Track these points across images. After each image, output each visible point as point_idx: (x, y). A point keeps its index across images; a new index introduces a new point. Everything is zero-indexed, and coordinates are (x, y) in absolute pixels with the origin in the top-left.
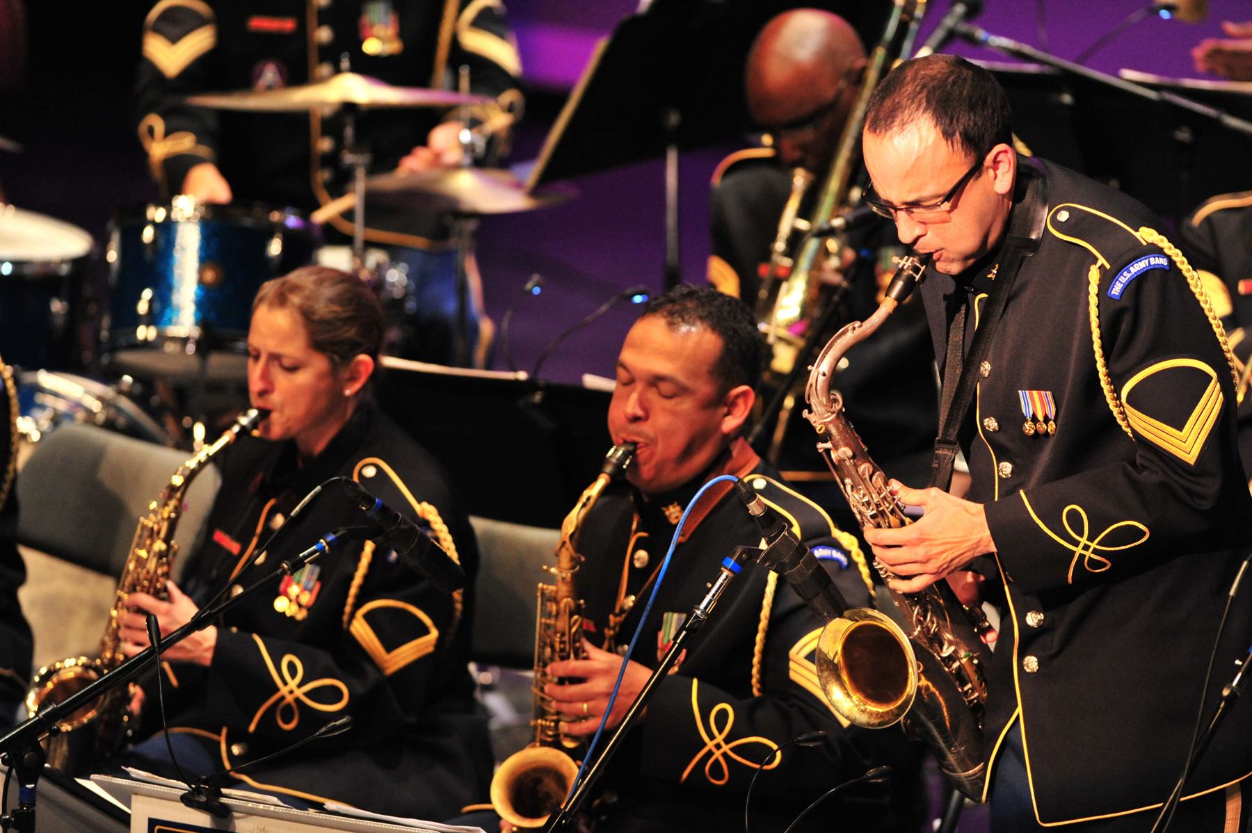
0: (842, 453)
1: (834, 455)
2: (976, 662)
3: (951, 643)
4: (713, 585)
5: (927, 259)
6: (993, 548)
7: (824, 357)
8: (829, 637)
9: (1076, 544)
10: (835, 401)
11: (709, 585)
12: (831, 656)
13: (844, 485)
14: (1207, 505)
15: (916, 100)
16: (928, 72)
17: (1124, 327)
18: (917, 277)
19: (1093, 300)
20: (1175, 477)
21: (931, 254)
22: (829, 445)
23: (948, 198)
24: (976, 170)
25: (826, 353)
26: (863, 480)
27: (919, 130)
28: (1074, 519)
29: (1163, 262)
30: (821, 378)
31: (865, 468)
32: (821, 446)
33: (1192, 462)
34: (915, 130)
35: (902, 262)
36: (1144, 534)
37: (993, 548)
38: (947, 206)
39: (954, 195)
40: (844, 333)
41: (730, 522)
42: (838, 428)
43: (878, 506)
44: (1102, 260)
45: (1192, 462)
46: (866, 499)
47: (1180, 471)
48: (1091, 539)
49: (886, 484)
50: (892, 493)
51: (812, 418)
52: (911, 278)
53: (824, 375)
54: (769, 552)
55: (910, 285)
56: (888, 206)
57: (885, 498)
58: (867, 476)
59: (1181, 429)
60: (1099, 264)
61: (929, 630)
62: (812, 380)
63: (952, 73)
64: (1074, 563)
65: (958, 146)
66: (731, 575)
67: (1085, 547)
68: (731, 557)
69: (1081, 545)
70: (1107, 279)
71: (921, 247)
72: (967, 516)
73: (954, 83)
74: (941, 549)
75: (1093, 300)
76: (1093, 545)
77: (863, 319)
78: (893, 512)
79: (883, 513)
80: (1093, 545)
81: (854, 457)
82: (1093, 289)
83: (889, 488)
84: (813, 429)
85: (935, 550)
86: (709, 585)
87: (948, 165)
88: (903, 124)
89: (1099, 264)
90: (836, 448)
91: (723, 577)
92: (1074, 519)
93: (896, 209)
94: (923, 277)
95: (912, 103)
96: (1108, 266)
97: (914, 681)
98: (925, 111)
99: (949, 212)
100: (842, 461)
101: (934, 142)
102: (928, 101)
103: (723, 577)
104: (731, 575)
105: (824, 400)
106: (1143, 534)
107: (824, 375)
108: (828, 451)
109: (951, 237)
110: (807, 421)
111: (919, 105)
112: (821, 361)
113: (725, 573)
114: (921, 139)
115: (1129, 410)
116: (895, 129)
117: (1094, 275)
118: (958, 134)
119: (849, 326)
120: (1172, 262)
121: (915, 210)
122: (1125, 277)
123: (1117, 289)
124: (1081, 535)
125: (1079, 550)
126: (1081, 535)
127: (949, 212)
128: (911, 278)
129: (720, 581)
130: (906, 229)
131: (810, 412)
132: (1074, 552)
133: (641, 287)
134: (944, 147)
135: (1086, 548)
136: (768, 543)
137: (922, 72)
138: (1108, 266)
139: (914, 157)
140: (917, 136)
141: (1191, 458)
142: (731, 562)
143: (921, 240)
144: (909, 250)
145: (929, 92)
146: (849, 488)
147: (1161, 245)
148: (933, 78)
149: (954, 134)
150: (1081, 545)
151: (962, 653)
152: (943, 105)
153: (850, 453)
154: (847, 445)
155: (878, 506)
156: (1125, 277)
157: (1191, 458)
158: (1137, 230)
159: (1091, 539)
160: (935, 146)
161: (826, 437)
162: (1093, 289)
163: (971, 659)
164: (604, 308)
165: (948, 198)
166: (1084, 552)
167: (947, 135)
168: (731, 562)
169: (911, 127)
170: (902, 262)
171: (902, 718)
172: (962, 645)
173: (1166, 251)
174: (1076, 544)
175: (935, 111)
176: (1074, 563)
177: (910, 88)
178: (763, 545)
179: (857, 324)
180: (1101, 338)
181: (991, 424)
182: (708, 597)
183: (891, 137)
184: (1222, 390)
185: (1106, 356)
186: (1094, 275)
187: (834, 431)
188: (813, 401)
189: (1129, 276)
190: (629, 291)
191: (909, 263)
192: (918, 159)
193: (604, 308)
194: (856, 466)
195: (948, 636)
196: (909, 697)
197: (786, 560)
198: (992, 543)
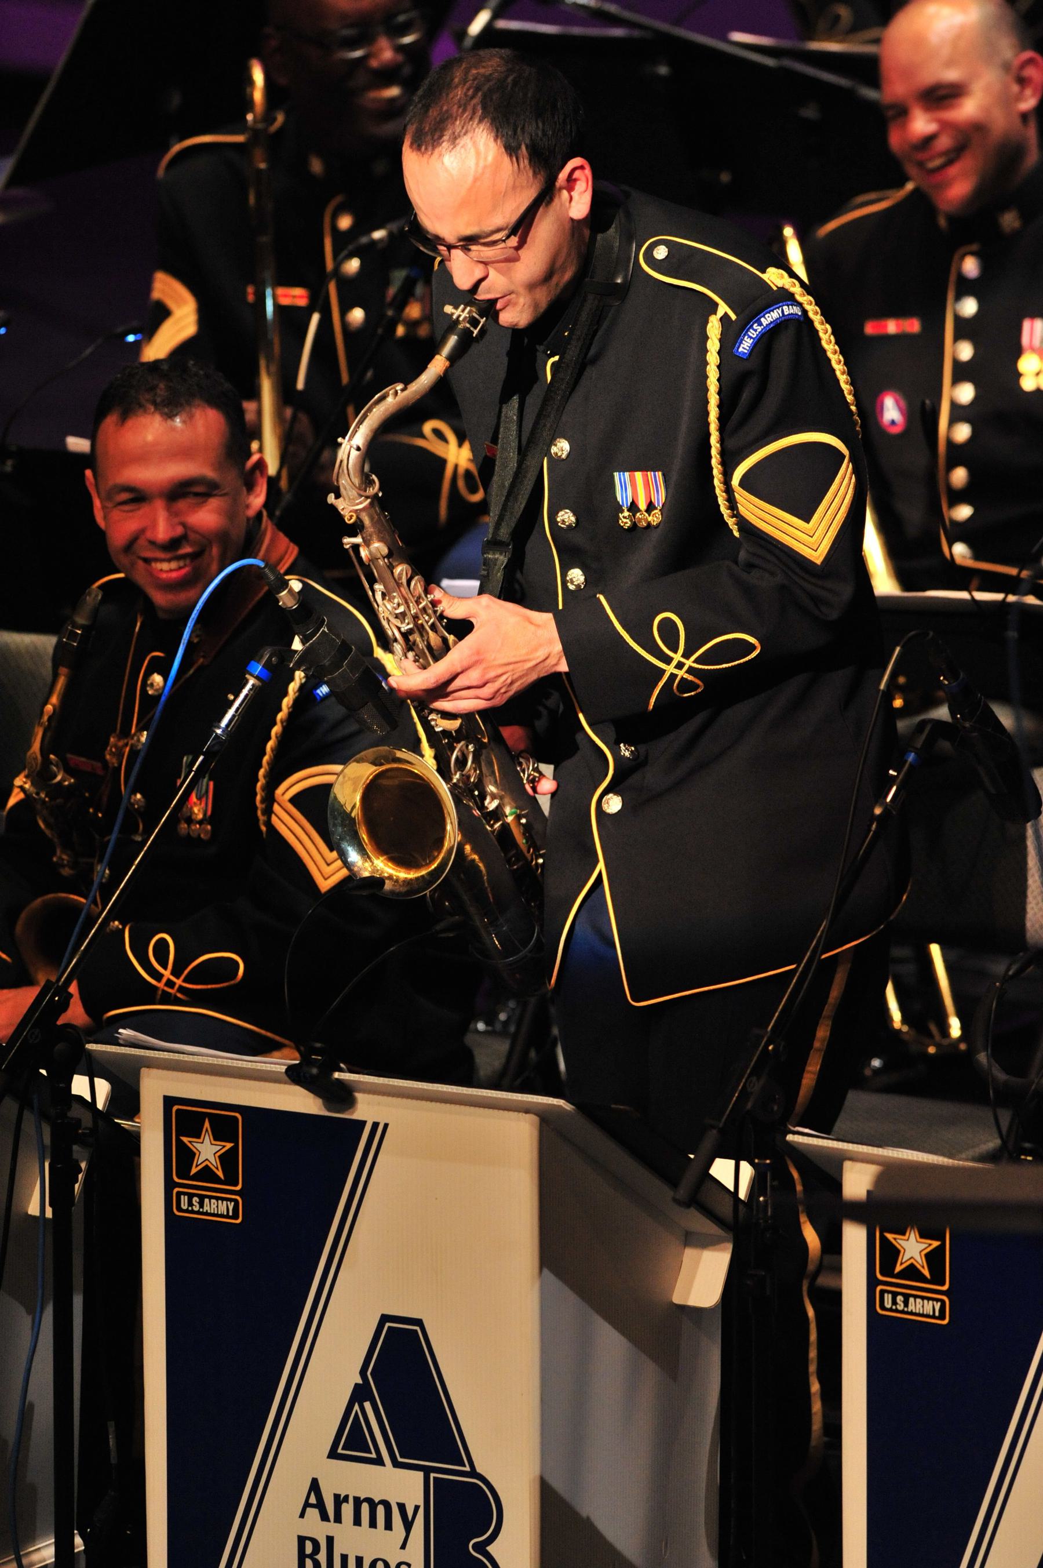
0: (373, 549)
1: (364, 553)
2: (524, 821)
3: (494, 797)
4: (236, 696)
5: (490, 309)
6: (563, 667)
7: (358, 426)
8: (349, 782)
9: (668, 660)
10: (372, 482)
11: (231, 697)
12: (348, 809)
13: (373, 591)
14: (834, 615)
15: (470, 108)
16: (482, 71)
17: (746, 396)
18: (476, 332)
19: (713, 358)
20: (797, 579)
21: (494, 301)
22: (358, 540)
23: (513, 232)
24: (546, 196)
25: (361, 422)
26: (399, 585)
27: (475, 144)
28: (668, 631)
29: (796, 310)
30: (354, 454)
31: (401, 569)
32: (348, 541)
33: (819, 562)
34: (470, 144)
35: (457, 313)
36: (754, 648)
37: (563, 667)
38: (514, 241)
39: (522, 227)
40: (383, 398)
41: (245, 620)
42: (372, 518)
43: (415, 618)
44: (723, 308)
45: (819, 562)
46: (401, 609)
47: (798, 570)
48: (686, 655)
49: (427, 592)
50: (434, 603)
51: (341, 505)
52: (467, 333)
53: (358, 449)
54: (306, 653)
55: (466, 341)
56: (434, 241)
57: (424, 610)
58: (404, 580)
59: (808, 522)
60: (720, 313)
61: (469, 777)
62: (342, 454)
63: (510, 71)
64: (661, 684)
65: (525, 162)
66: (258, 683)
67: (678, 665)
68: (258, 662)
69: (674, 663)
70: (731, 333)
71: (482, 295)
72: (532, 628)
73: (515, 83)
74: (500, 671)
75: (713, 358)
76: (689, 663)
77: (407, 382)
78: (433, 627)
79: (421, 629)
80: (689, 663)
81: (390, 555)
82: (713, 345)
83: (430, 597)
84: (341, 517)
85: (492, 674)
86: (231, 697)
87: (514, 187)
88: (454, 139)
89: (720, 313)
90: (367, 543)
91: (249, 686)
92: (668, 628)
93: (450, 247)
94: (483, 332)
95: (464, 111)
96: (733, 317)
97: (452, 834)
98: (480, 121)
99: (518, 248)
100: (373, 559)
101: (495, 158)
102: (484, 108)
103: (249, 686)
104: (258, 683)
105: (357, 481)
106: (753, 648)
107: (358, 449)
108: (356, 547)
109: (511, 284)
110: (333, 508)
111: (474, 113)
112: (355, 432)
113: (252, 681)
114: (478, 153)
115: (743, 497)
116: (445, 144)
117: (714, 328)
118: (523, 147)
119: (390, 390)
120: (805, 312)
121: (473, 248)
122: (756, 331)
123: (745, 346)
124: (675, 650)
125: (670, 669)
126: (675, 650)
127: (518, 248)
128: (467, 333)
129: (245, 691)
130: (462, 270)
131: (338, 496)
132: (664, 671)
133: (135, 324)
134: (507, 165)
135: (680, 665)
136: (303, 642)
137: (474, 72)
138: (733, 317)
139: (470, 179)
140: (473, 151)
141: (818, 556)
142: (257, 668)
143: (483, 284)
144: (469, 296)
145: (484, 97)
146: (379, 596)
147: (792, 290)
148: (488, 78)
149: (519, 147)
150: (674, 663)
151: (508, 810)
152: (504, 115)
153: (385, 551)
154: (381, 540)
155: (415, 618)
156: (756, 331)
157: (818, 556)
158: (764, 272)
159: (686, 655)
160: (496, 167)
161: (355, 529)
162: (713, 345)
163: (518, 817)
164: (89, 351)
165: (513, 232)
166: (676, 671)
167: (511, 150)
168: (257, 668)
169: (465, 141)
170: (457, 313)
171: (427, 892)
172: (507, 800)
173: (798, 298)
174: (668, 660)
175: (493, 121)
176: (661, 684)
177: (459, 93)
178: (297, 645)
179: (399, 387)
180: (720, 406)
181: (566, 517)
182: (231, 712)
183: (441, 155)
184: (854, 471)
185: (721, 430)
186: (714, 328)
187: (367, 521)
188: (344, 482)
189: (759, 329)
190: (120, 330)
191: (465, 314)
192: (476, 180)
193: (89, 351)
194: (391, 568)
195: (492, 788)
196: (451, 849)
197: (326, 662)
198: (564, 661)
